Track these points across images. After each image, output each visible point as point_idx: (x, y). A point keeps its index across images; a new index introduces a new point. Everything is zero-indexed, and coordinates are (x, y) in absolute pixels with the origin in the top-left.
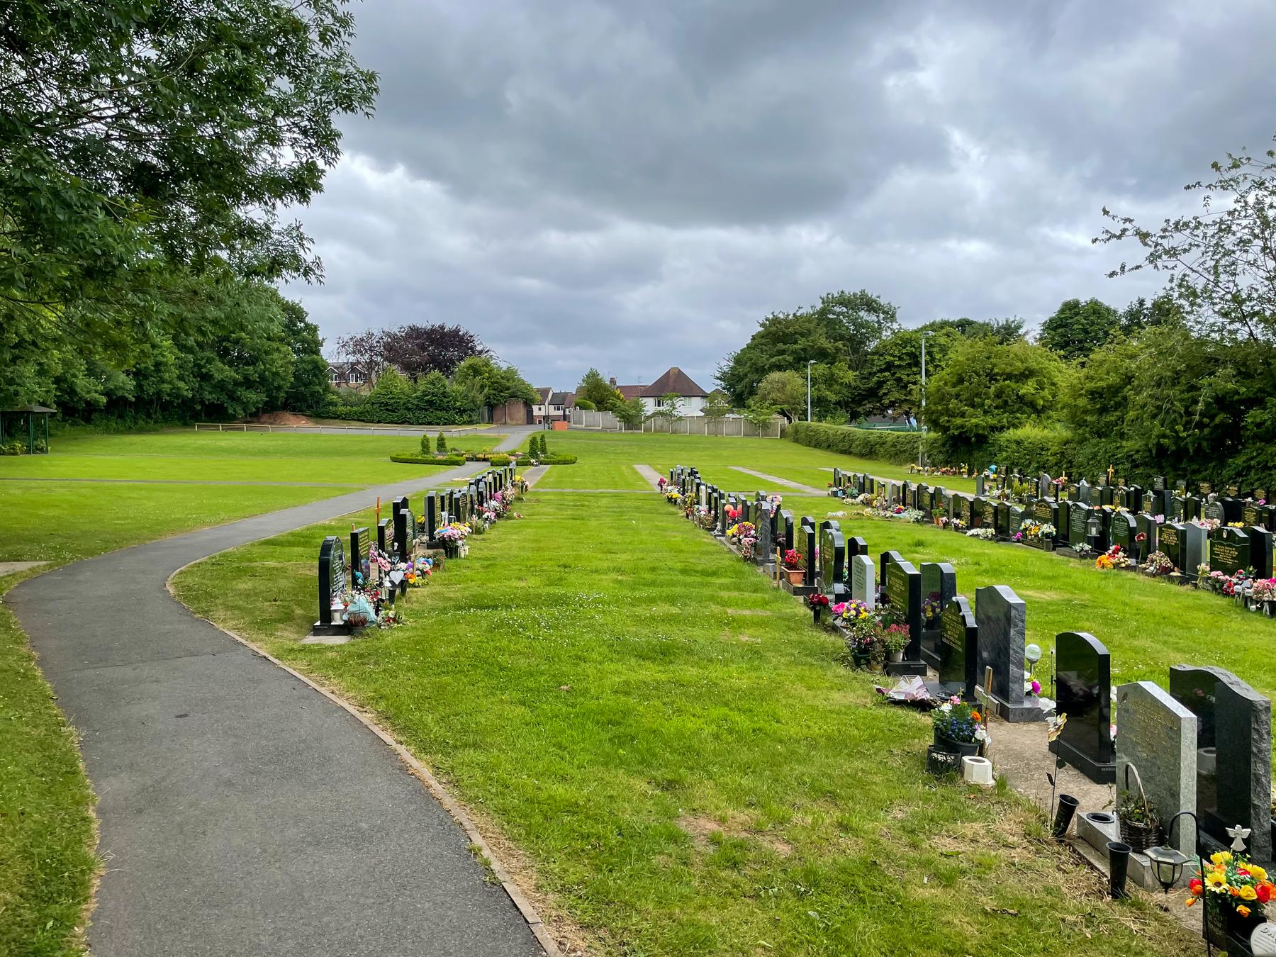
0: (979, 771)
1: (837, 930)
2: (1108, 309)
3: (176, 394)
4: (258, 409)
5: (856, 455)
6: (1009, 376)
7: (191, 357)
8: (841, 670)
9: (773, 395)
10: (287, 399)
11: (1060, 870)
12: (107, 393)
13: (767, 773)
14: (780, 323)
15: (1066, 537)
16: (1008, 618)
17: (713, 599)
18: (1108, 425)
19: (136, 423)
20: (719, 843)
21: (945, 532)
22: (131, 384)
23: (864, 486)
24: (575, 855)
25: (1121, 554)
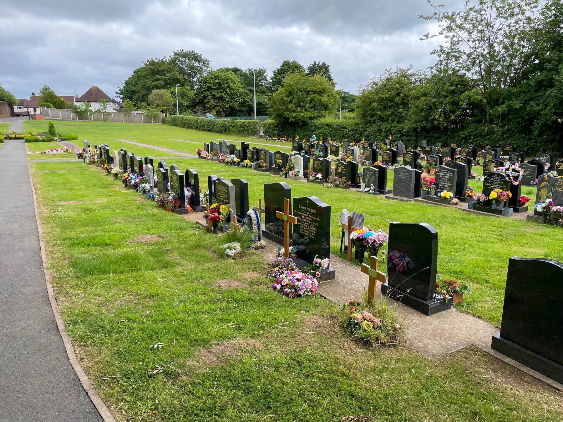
6: (315, 92)
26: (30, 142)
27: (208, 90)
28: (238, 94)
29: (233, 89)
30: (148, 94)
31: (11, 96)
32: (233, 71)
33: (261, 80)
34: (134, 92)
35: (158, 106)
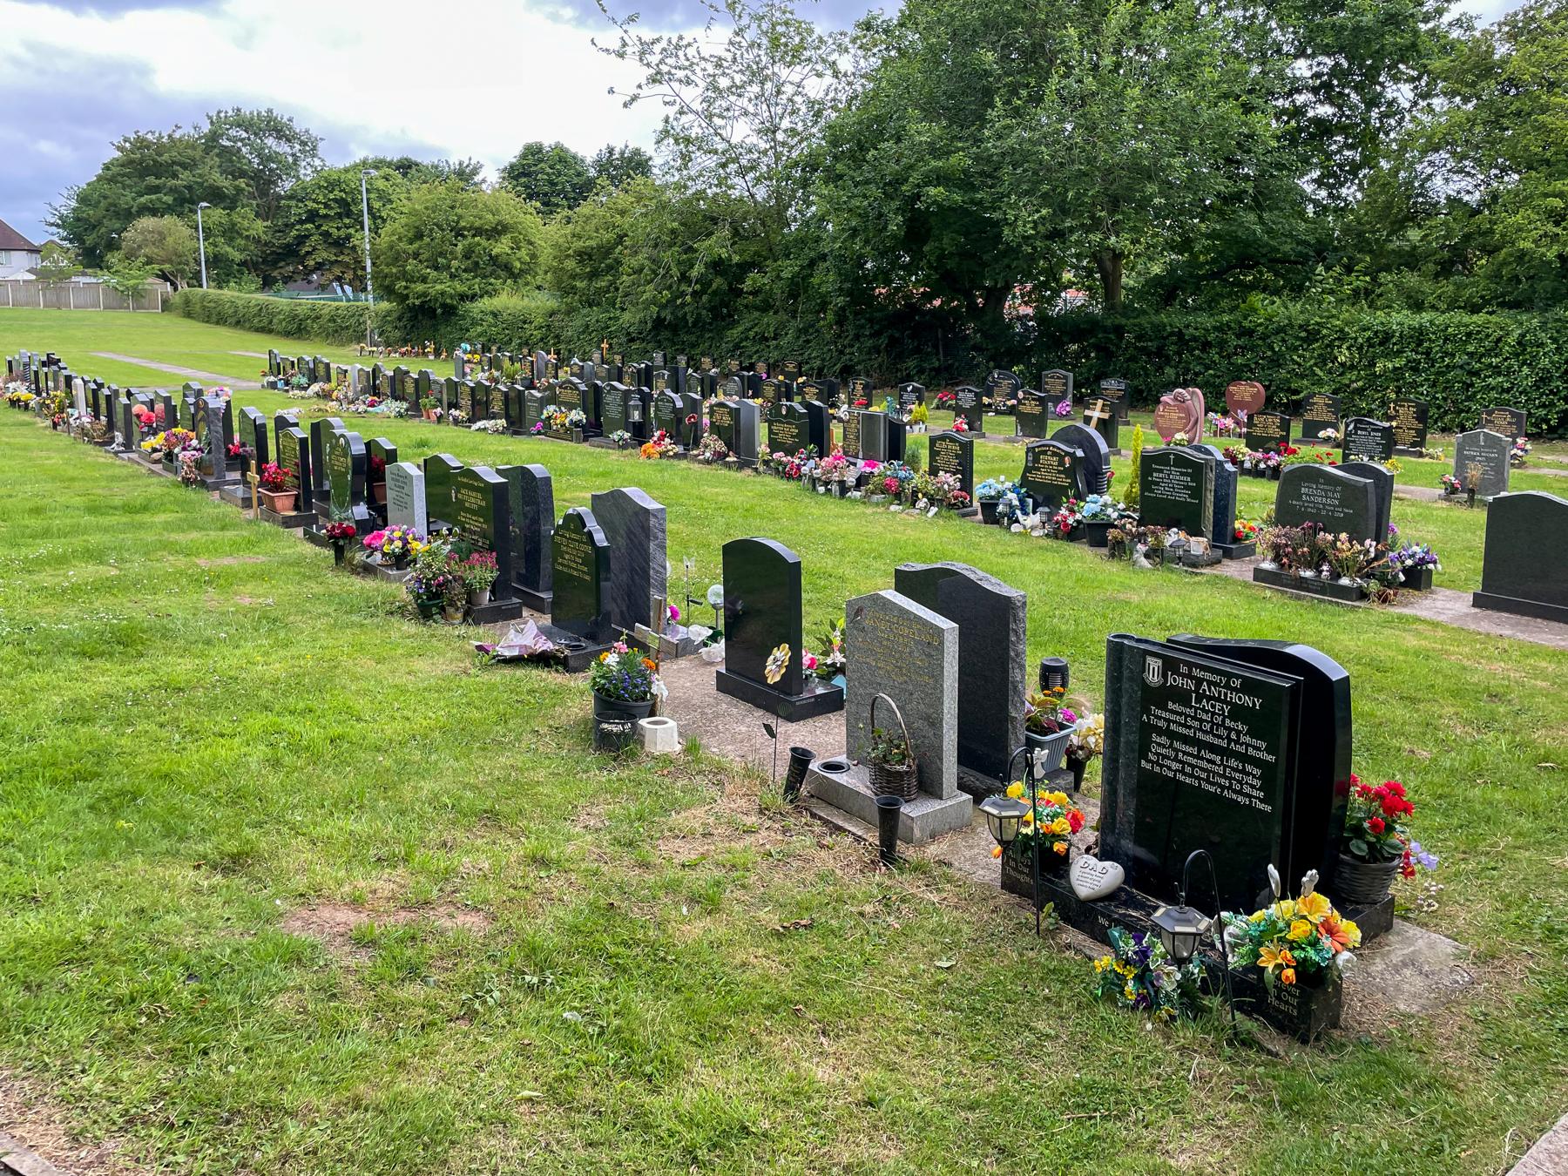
0: (662, 735)
1: (618, 1031)
2: (574, 157)
5: (278, 333)
6: (478, 232)
8: (409, 627)
11: (823, 847)
13: (382, 803)
15: (598, 425)
16: (646, 530)
17: (167, 546)
18: (599, 291)
20: (373, 943)
21: (442, 427)
23: (316, 373)
24: (119, 1044)
25: (667, 440)
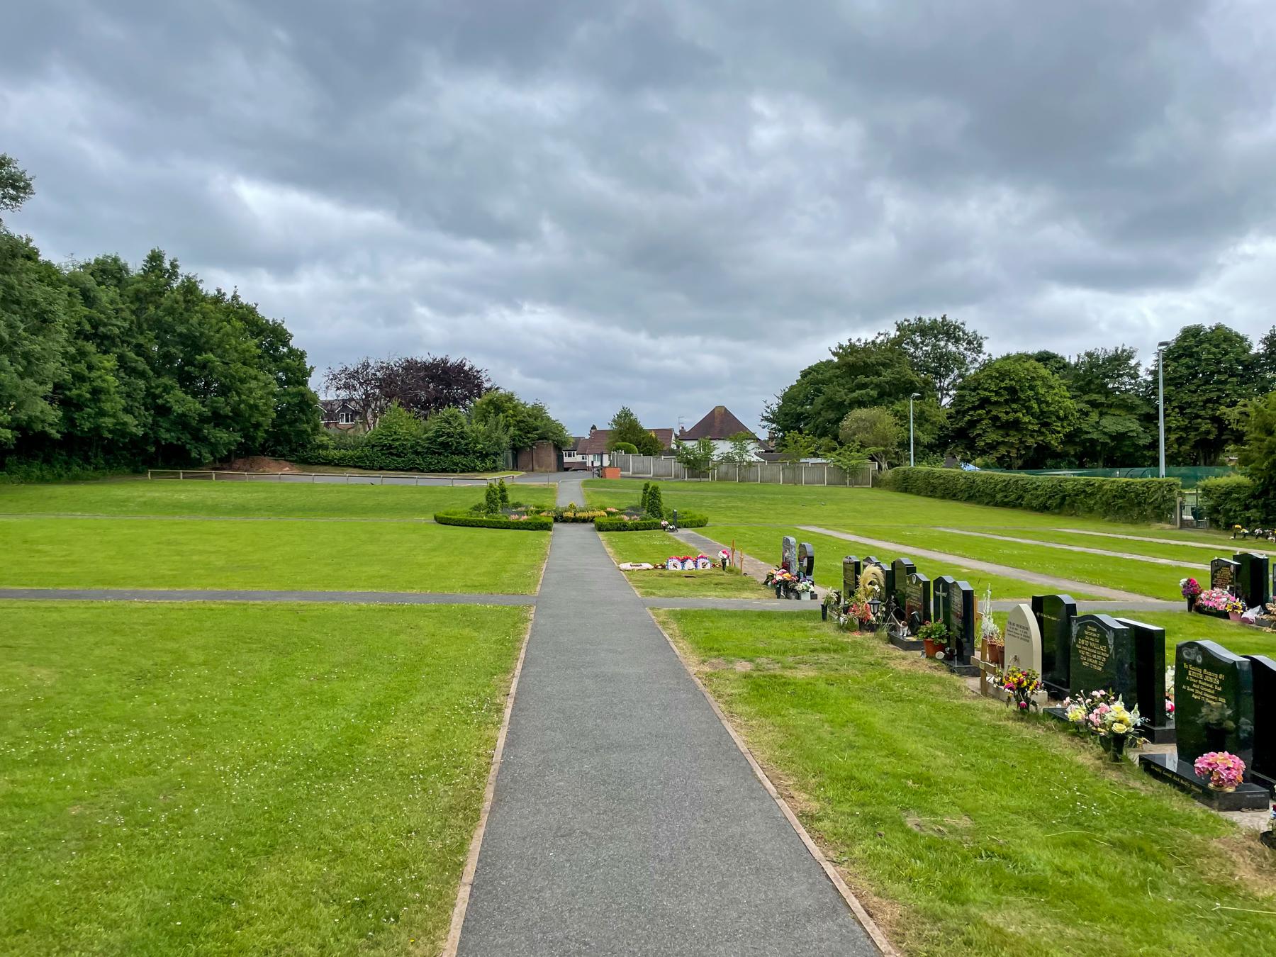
2: (1237, 336)
3: (121, 431)
4: (229, 451)
7: (142, 383)
9: (859, 436)
10: (266, 441)
12: (16, 426)
14: (857, 351)
19: (69, 470)
22: (53, 414)
26: (608, 530)
27: (981, 407)
28: (1061, 413)
29: (1047, 403)
30: (840, 419)
31: (559, 429)
32: (1038, 360)
33: (1122, 376)
34: (799, 417)
35: (863, 446)
